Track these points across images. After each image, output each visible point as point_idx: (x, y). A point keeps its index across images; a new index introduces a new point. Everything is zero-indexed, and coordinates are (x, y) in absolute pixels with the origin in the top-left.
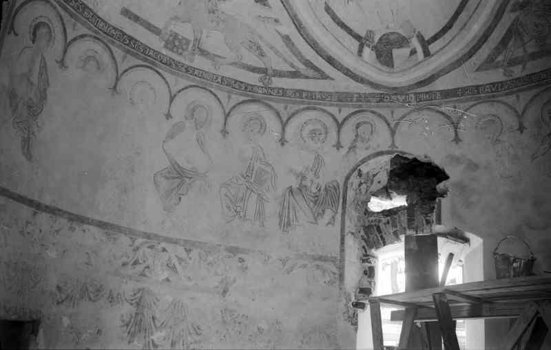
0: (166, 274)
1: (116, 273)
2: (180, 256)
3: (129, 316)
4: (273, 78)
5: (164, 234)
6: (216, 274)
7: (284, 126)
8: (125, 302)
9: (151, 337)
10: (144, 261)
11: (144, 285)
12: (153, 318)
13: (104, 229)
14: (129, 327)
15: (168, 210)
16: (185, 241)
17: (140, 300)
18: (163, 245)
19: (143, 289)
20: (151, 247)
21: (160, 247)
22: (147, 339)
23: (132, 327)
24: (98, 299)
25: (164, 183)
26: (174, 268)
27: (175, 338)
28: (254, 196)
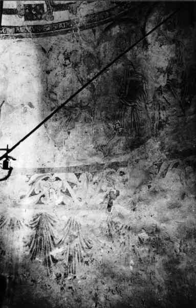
2: (71, 181)
6: (101, 191)
9: (51, 253)
10: (40, 192)
11: (43, 211)
12: (52, 238)
17: (39, 223)
21: (53, 178)
22: (47, 255)
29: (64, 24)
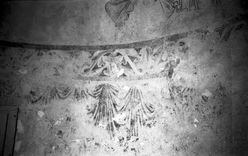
0: (122, 71)
1: (80, 77)
3: (93, 106)
5: (117, 43)
8: (88, 96)
9: (113, 119)
10: (102, 66)
13: (68, 50)
14: (95, 114)
15: (119, 25)
16: (135, 44)
17: (102, 93)
18: (117, 51)
19: (104, 85)
20: (107, 55)
21: (115, 53)
22: (110, 121)
23: (97, 114)
24: (66, 97)
25: (114, 9)
26: (128, 66)
27: (133, 118)
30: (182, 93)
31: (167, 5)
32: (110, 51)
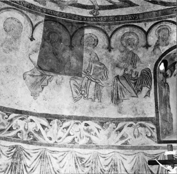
4: (99, 11)
7: (109, 39)
10: (17, 128)
18: (31, 117)
28: (93, 84)
29: (52, 12)
30: (85, 163)
31: (108, 159)
32: (25, 116)
